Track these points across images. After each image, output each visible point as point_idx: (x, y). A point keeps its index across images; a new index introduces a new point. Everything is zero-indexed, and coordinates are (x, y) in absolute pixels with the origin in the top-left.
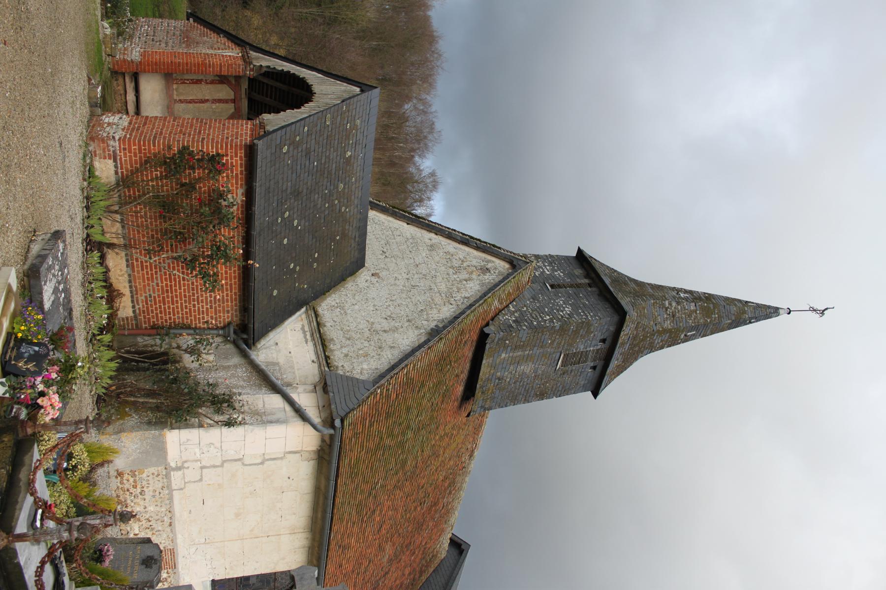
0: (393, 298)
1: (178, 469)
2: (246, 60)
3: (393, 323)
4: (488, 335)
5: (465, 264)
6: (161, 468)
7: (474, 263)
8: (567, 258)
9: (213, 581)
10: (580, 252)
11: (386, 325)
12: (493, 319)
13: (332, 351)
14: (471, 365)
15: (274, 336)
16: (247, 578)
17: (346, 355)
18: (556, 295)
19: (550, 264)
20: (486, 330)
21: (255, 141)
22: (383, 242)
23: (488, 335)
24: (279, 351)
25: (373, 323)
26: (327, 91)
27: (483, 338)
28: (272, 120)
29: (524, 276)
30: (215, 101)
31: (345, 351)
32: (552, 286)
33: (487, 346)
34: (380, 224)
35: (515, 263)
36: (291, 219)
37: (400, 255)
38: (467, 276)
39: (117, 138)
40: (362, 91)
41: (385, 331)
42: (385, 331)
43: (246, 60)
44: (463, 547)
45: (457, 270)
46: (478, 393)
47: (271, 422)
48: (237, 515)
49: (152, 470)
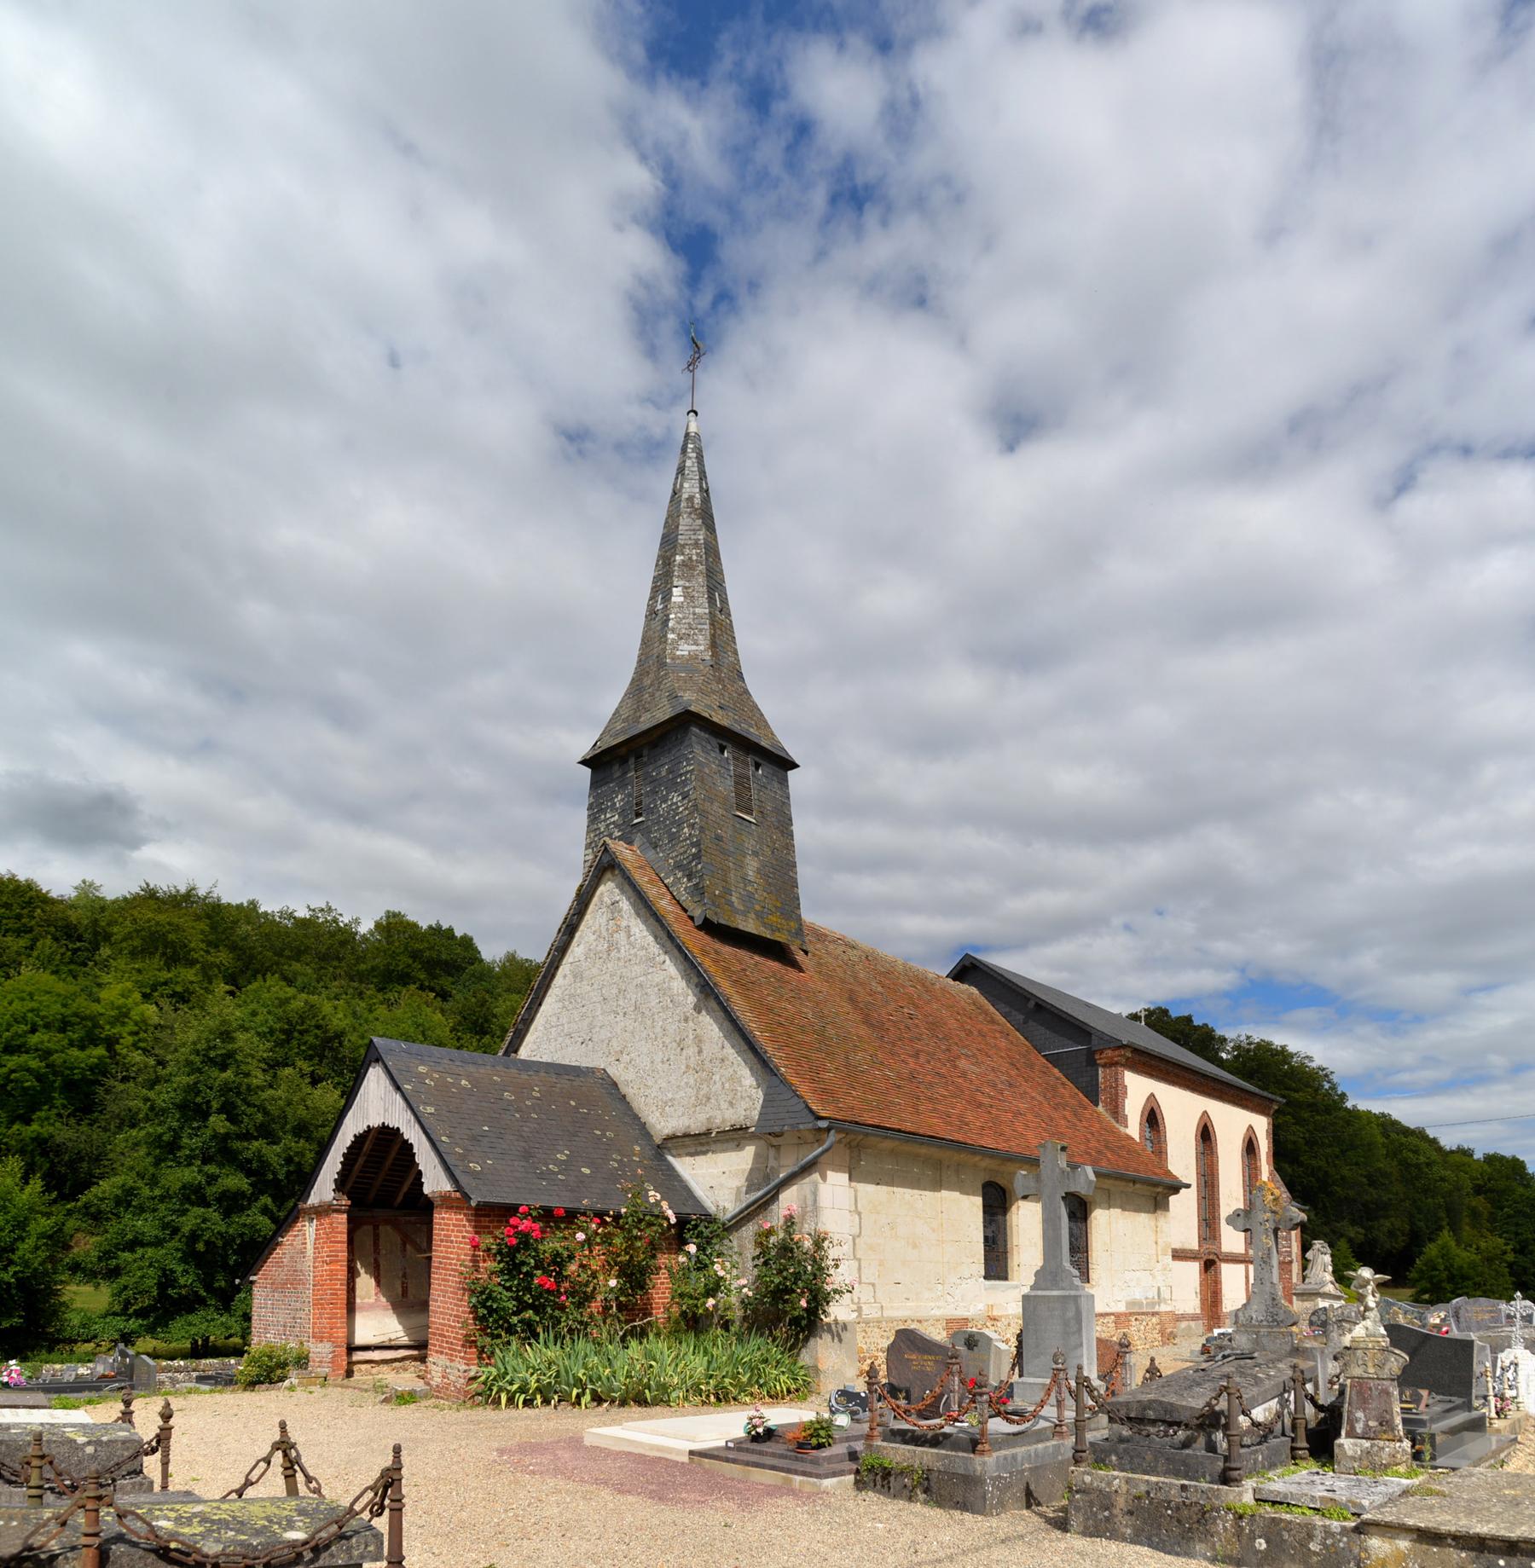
0: (629, 1022)
1: (859, 1310)
2: (322, 1211)
3: (689, 1041)
4: (706, 919)
5: (605, 934)
6: (858, 1328)
7: (603, 920)
8: (595, 784)
9: (985, 1278)
10: (584, 762)
11: (691, 1051)
12: (685, 911)
13: (724, 1121)
14: (743, 943)
15: (700, 1192)
16: (986, 1239)
17: (731, 1104)
18: (651, 811)
19: (604, 811)
20: (699, 922)
21: (473, 1204)
22: (568, 1041)
23: (706, 919)
24: (721, 1185)
25: (688, 1067)
26: (376, 1104)
27: (710, 927)
28: (434, 1182)
29: (621, 850)
30: (376, 1250)
31: (724, 1105)
32: (638, 815)
33: (722, 921)
34: (542, 1043)
35: (604, 867)
36: (557, 1162)
37: (587, 1021)
38: (623, 934)
39: (465, 1367)
40: (378, 1059)
41: (700, 1052)
42: (700, 1052)
43: (322, 1211)
44: (967, 963)
45: (612, 947)
46: (780, 937)
47: (815, 1201)
48: (915, 1246)
49: (859, 1338)
